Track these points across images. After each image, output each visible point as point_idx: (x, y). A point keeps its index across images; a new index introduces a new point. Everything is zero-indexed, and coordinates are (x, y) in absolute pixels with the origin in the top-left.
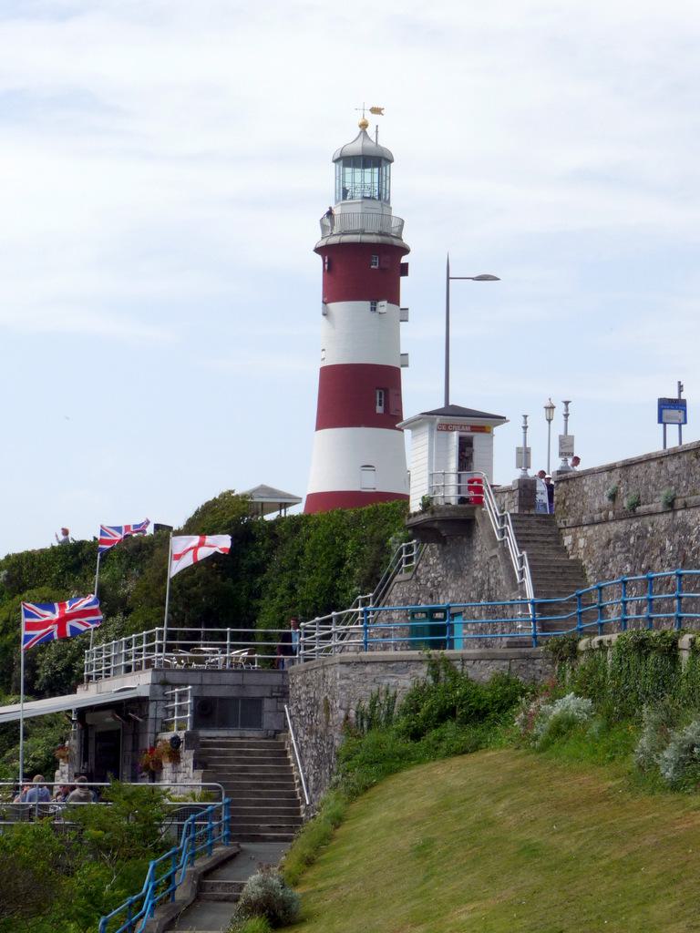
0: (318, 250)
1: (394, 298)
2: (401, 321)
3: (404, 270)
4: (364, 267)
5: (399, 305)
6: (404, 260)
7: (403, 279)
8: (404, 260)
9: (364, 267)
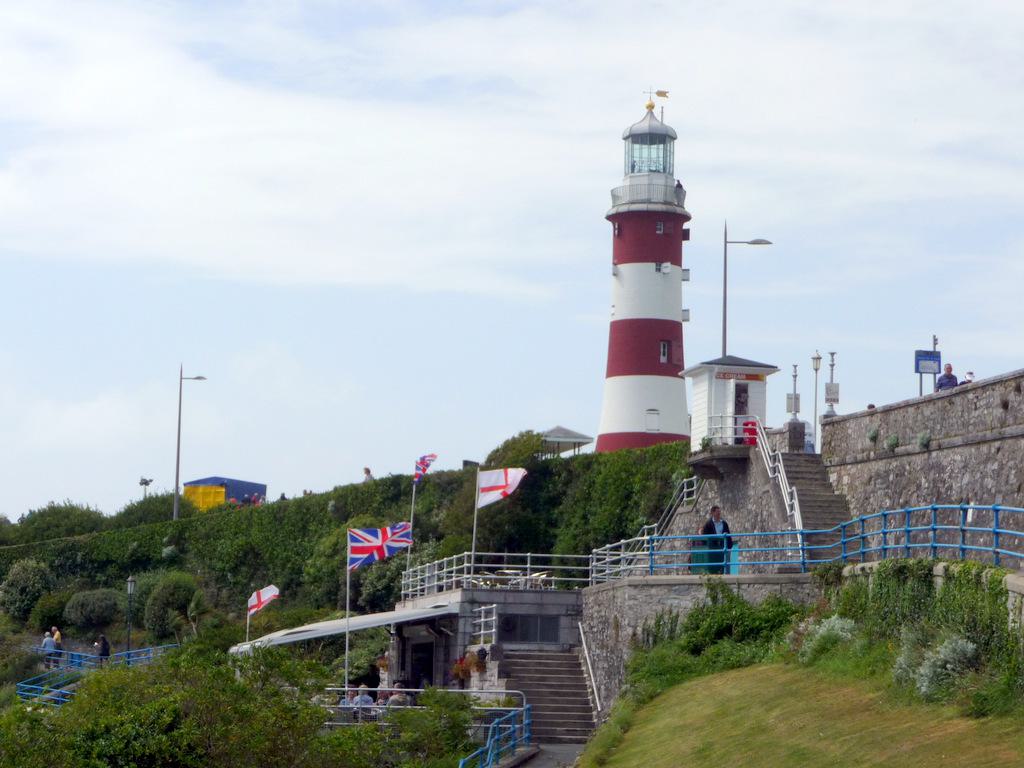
0: (610, 218)
1: (676, 260)
2: (684, 280)
3: (686, 235)
4: (651, 233)
5: (680, 265)
6: (686, 226)
7: (684, 243)
8: (686, 226)
9: (651, 233)
